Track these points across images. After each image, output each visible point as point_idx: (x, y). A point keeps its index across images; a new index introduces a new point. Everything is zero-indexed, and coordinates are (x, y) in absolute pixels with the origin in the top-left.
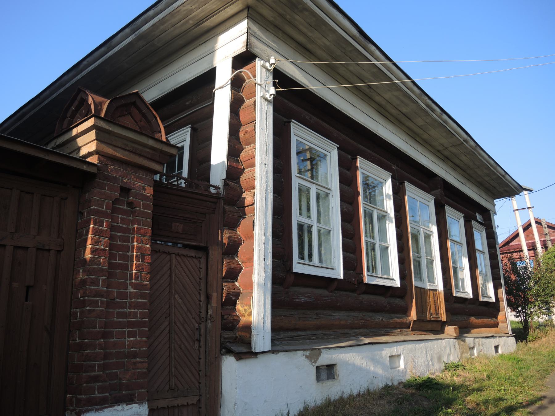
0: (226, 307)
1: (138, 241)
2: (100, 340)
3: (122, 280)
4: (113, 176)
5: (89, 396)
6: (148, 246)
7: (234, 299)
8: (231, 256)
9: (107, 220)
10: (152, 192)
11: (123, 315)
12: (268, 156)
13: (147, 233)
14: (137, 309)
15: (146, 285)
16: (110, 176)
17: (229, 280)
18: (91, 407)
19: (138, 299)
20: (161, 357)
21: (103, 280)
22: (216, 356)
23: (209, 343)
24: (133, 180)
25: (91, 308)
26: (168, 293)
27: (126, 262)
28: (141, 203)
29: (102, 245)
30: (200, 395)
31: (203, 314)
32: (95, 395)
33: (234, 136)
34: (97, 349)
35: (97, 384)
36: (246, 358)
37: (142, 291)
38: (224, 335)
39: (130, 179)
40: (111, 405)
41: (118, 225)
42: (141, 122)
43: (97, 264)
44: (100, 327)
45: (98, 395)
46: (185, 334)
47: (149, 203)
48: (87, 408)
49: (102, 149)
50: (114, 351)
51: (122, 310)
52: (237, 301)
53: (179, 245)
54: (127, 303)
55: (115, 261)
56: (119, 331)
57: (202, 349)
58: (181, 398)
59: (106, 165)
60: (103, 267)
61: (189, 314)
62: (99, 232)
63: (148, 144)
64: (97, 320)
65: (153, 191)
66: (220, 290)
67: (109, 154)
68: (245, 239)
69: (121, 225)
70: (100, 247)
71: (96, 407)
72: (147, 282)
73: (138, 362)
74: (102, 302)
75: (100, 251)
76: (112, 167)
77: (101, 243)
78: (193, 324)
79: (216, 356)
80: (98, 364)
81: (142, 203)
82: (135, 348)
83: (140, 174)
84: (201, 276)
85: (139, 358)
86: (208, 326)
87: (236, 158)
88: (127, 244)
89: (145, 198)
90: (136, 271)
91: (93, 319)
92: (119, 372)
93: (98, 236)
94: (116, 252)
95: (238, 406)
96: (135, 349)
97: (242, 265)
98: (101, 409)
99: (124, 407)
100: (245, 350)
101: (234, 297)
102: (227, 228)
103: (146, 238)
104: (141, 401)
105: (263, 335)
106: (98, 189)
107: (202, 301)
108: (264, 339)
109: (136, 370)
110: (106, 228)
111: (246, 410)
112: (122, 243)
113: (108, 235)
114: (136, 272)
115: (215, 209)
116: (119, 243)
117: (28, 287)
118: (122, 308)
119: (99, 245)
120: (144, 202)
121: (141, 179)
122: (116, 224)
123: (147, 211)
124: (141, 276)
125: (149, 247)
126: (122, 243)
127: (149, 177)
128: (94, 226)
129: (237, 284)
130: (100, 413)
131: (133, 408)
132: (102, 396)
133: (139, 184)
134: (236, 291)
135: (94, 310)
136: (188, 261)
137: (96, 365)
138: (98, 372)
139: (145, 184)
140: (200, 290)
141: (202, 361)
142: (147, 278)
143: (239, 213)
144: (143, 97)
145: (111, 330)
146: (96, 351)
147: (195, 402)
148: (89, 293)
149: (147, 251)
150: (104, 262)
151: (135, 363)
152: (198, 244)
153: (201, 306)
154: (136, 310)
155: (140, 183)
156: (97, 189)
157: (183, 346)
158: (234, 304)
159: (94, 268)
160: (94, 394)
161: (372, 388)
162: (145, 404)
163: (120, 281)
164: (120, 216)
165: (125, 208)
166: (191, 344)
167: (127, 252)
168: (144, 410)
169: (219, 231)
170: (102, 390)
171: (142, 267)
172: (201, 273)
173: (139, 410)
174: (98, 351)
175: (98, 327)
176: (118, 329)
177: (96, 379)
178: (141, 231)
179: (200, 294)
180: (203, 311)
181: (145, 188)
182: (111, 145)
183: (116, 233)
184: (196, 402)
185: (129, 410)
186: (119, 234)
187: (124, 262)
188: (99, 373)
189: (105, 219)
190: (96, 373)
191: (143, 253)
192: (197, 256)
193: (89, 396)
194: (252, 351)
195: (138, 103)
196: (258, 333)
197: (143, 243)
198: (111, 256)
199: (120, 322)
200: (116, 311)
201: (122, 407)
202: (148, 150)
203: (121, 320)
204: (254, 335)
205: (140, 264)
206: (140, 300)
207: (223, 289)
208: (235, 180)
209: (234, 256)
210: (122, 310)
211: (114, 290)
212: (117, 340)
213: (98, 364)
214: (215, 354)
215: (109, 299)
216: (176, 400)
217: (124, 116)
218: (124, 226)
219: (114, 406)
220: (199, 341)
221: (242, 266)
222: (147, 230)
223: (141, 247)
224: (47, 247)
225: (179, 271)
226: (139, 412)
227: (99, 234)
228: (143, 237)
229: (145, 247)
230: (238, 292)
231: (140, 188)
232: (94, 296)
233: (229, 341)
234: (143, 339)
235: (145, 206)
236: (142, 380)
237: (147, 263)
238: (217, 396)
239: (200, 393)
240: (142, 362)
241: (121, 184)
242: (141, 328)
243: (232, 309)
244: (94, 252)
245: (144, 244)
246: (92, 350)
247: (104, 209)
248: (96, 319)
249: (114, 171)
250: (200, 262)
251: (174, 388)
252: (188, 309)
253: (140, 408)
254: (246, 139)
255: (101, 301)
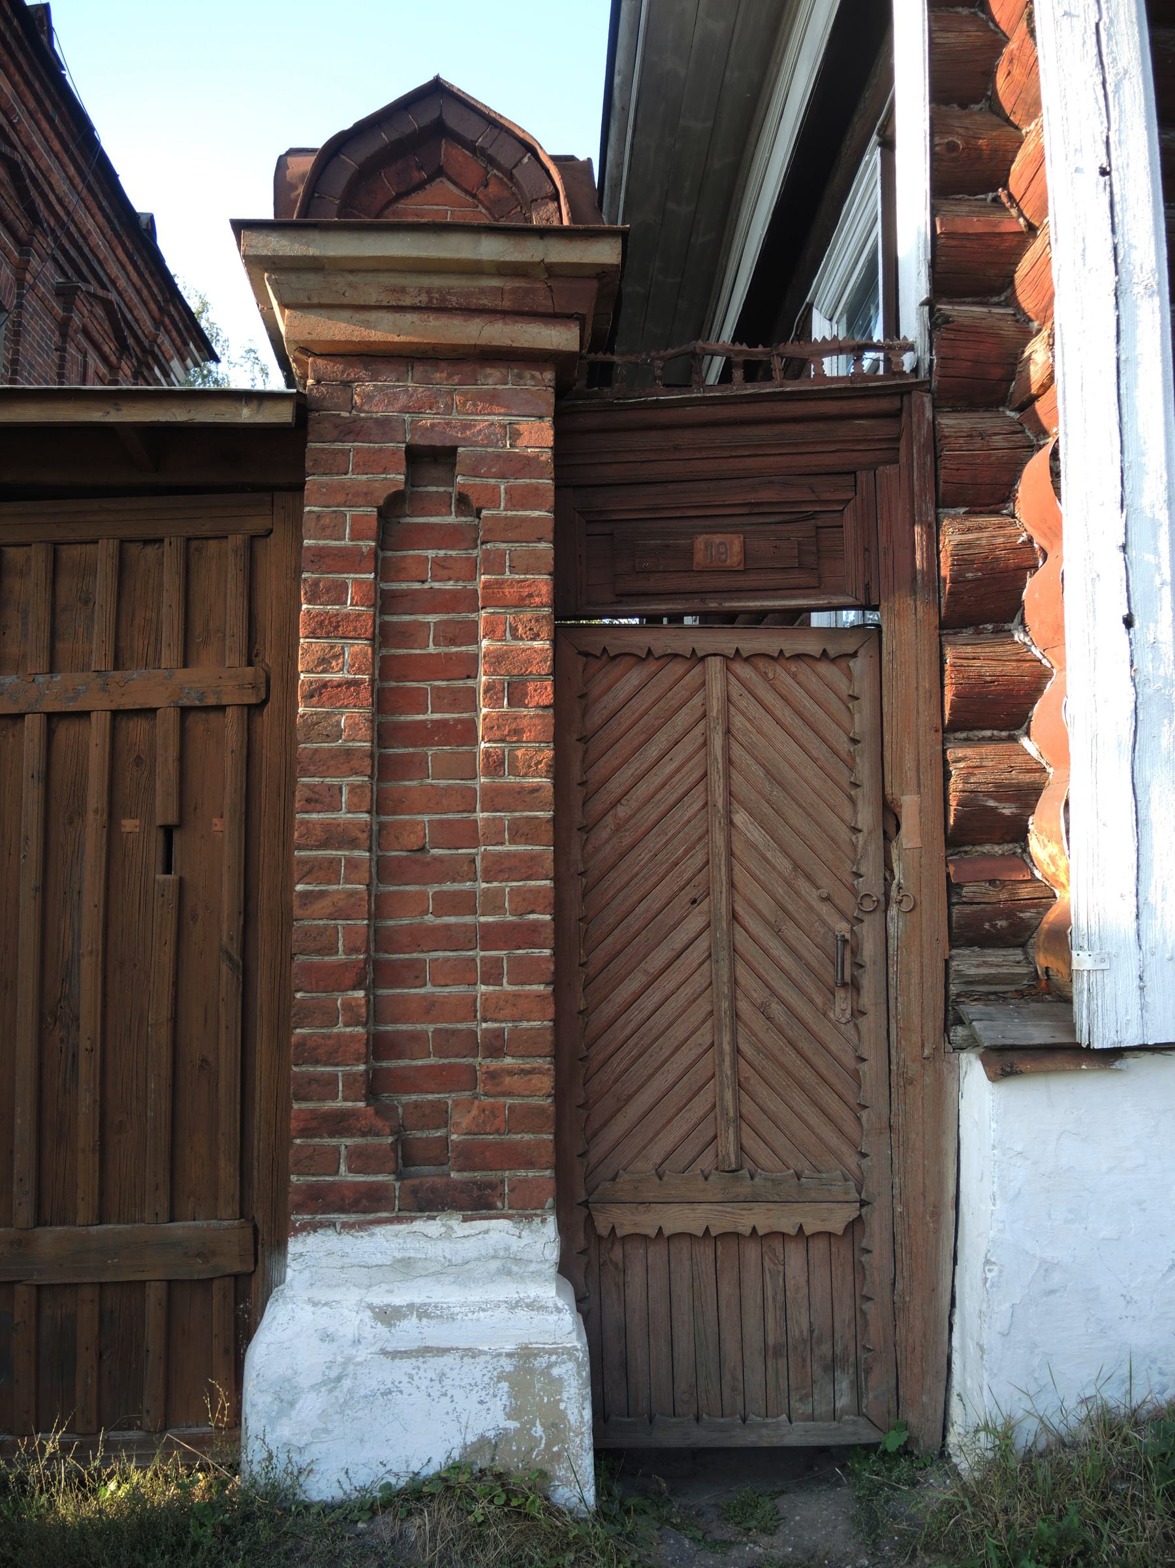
0: (979, 848)
1: (493, 631)
2: (350, 993)
3: (450, 781)
4: (374, 415)
5: (314, 1179)
6: (537, 644)
7: (1014, 816)
8: (990, 627)
9: (357, 576)
10: (548, 437)
11: (465, 902)
12: (1119, 130)
13: (530, 596)
14: (501, 881)
15: (536, 790)
16: (362, 419)
17: (988, 733)
18: (325, 1216)
19: (502, 844)
20: (677, 1049)
21: (353, 789)
22: (926, 1052)
23: (897, 999)
24: (459, 412)
25: (310, 887)
26: (699, 810)
27: (465, 715)
28: (502, 487)
29: (345, 668)
30: (863, 1203)
31: (871, 883)
32: (337, 1178)
33: (977, 103)
34: (340, 1025)
35: (343, 1140)
36: (1035, 1072)
37: (517, 814)
38: (961, 967)
39: (449, 409)
40: (401, 1214)
41: (426, 586)
42: (486, 186)
43: (327, 735)
44: (350, 950)
45: (350, 1179)
46: (787, 961)
47: (534, 481)
48: (309, 1217)
49: (309, 333)
50: (431, 1028)
51: (456, 887)
52: (1027, 821)
53: (688, 620)
54: (474, 861)
55: (421, 717)
56: (447, 960)
57: (870, 1023)
58: (770, 1206)
59: (347, 384)
60: (351, 744)
61: (802, 884)
62: (330, 622)
63: (479, 257)
64: (336, 927)
65: (552, 432)
66: (932, 779)
67: (340, 341)
68: (1045, 545)
69: (436, 585)
70: (337, 677)
71: (344, 1217)
72: (541, 777)
73: (511, 1072)
74: (352, 864)
75: (336, 691)
76: (369, 386)
77: (340, 661)
78: (824, 923)
79: (926, 1052)
80: (346, 1075)
81: (505, 489)
82: (495, 1021)
83: (490, 381)
84: (857, 731)
85: (513, 1056)
86: (892, 929)
87: (991, 195)
88: (463, 648)
89: (526, 465)
90: (489, 741)
91: (321, 922)
92: (453, 1101)
93: (326, 638)
94: (421, 685)
95: (1001, 1272)
96: (496, 1025)
97: (1044, 661)
98: (362, 1226)
99: (451, 1228)
100: (1039, 1034)
101: (1007, 805)
102: (963, 510)
103: (529, 615)
104: (527, 1212)
105: (1136, 973)
106: (319, 475)
107: (865, 830)
108: (1142, 989)
109: (502, 1100)
110: (356, 605)
111: (1052, 1292)
112: (446, 650)
113: (366, 631)
114: (487, 745)
115: (897, 440)
116: (432, 649)
117: (168, 831)
118: (454, 880)
119: (333, 668)
120: (512, 482)
121: (493, 398)
122: (417, 586)
123: (527, 513)
124: (513, 760)
125: (542, 650)
126: (446, 650)
127: (529, 382)
128: (310, 607)
129: (1029, 745)
130: (357, 1237)
131: (491, 1233)
132: (364, 1182)
133: (487, 420)
134: (1021, 776)
135: (322, 894)
136: (794, 676)
137: (337, 1076)
138: (345, 1099)
139: (514, 412)
140: (856, 785)
141: (871, 1070)
142: (540, 762)
143: (1023, 432)
144: (459, 90)
145: (415, 955)
146: (335, 1030)
147: (838, 1227)
148: (301, 836)
149: (534, 662)
150: (354, 726)
151: (493, 1075)
152: (821, 602)
153: (859, 849)
154: (495, 884)
155: (490, 418)
156: (315, 477)
157: (776, 1009)
158: (1018, 833)
159: (316, 750)
160: (337, 1172)
161: (1114, 1396)
162: (544, 1221)
163: (443, 783)
164: (431, 553)
165: (452, 519)
166: (819, 1000)
167: (468, 677)
168: (539, 1246)
169: (917, 529)
170: (362, 1160)
171: (514, 726)
172: (857, 716)
173: (515, 1244)
174: (343, 1030)
175: (341, 948)
176: (440, 954)
177: (339, 1123)
178: (506, 591)
179: (853, 801)
180: (871, 867)
181: (517, 430)
182: (342, 307)
183: (421, 618)
184: (843, 1225)
185: (474, 1239)
186: (432, 618)
187: (456, 716)
188: (350, 1104)
189: (352, 576)
190: (339, 1104)
191: (516, 672)
192: (832, 653)
193: (314, 1179)
194: (1078, 1040)
195: (453, 120)
196: (1103, 961)
197: (515, 637)
198: (382, 701)
199: (448, 927)
200: (432, 889)
201: (443, 1225)
202: (495, 282)
203: (452, 920)
204: (1085, 973)
205: (503, 716)
206: (513, 848)
207: (947, 776)
208: (999, 294)
209: (1011, 626)
210: (456, 887)
211: (419, 817)
212: (439, 989)
213: (346, 1075)
214: (923, 1046)
215: (402, 850)
216: (744, 1212)
217: (420, 186)
218: (449, 585)
219: (412, 1219)
220: (854, 986)
221: (1049, 665)
222: (529, 586)
223: (506, 650)
224: (211, 701)
225: (749, 720)
226: (514, 1248)
227: (328, 633)
228: (515, 613)
229: (524, 651)
230: (1033, 783)
231: (490, 435)
232: (324, 845)
233: (995, 993)
234: (527, 988)
235: (518, 499)
236: (527, 1137)
237: (538, 707)
238: (937, 1213)
239: (863, 1196)
240: (523, 1072)
241: (408, 437)
242: (520, 948)
243: (1014, 853)
244: (312, 696)
245: (522, 639)
246: (322, 1027)
247: (347, 542)
248: (333, 922)
249: (377, 399)
250: (849, 675)
251: (733, 1166)
252: (796, 866)
253: (520, 1237)
254: (1018, 92)
255: (349, 860)
